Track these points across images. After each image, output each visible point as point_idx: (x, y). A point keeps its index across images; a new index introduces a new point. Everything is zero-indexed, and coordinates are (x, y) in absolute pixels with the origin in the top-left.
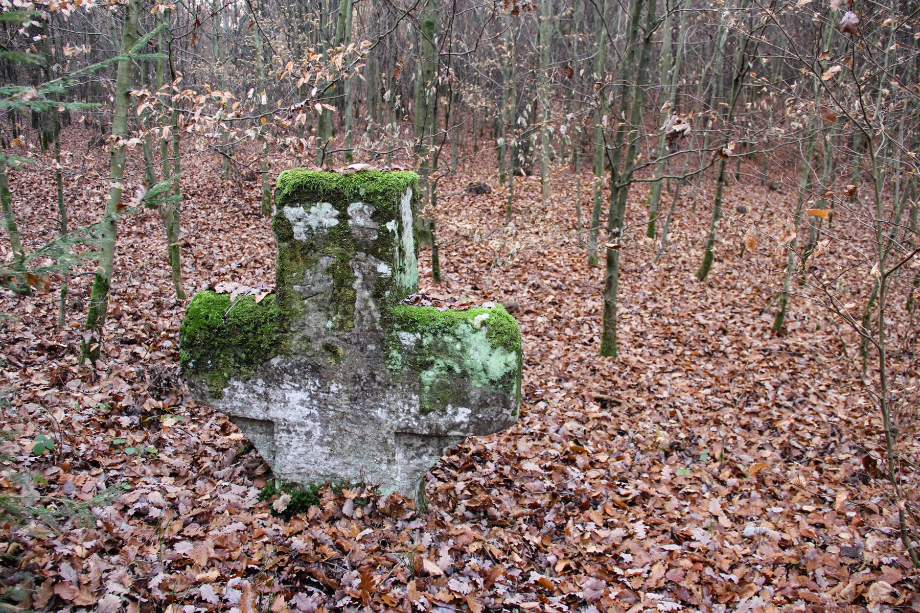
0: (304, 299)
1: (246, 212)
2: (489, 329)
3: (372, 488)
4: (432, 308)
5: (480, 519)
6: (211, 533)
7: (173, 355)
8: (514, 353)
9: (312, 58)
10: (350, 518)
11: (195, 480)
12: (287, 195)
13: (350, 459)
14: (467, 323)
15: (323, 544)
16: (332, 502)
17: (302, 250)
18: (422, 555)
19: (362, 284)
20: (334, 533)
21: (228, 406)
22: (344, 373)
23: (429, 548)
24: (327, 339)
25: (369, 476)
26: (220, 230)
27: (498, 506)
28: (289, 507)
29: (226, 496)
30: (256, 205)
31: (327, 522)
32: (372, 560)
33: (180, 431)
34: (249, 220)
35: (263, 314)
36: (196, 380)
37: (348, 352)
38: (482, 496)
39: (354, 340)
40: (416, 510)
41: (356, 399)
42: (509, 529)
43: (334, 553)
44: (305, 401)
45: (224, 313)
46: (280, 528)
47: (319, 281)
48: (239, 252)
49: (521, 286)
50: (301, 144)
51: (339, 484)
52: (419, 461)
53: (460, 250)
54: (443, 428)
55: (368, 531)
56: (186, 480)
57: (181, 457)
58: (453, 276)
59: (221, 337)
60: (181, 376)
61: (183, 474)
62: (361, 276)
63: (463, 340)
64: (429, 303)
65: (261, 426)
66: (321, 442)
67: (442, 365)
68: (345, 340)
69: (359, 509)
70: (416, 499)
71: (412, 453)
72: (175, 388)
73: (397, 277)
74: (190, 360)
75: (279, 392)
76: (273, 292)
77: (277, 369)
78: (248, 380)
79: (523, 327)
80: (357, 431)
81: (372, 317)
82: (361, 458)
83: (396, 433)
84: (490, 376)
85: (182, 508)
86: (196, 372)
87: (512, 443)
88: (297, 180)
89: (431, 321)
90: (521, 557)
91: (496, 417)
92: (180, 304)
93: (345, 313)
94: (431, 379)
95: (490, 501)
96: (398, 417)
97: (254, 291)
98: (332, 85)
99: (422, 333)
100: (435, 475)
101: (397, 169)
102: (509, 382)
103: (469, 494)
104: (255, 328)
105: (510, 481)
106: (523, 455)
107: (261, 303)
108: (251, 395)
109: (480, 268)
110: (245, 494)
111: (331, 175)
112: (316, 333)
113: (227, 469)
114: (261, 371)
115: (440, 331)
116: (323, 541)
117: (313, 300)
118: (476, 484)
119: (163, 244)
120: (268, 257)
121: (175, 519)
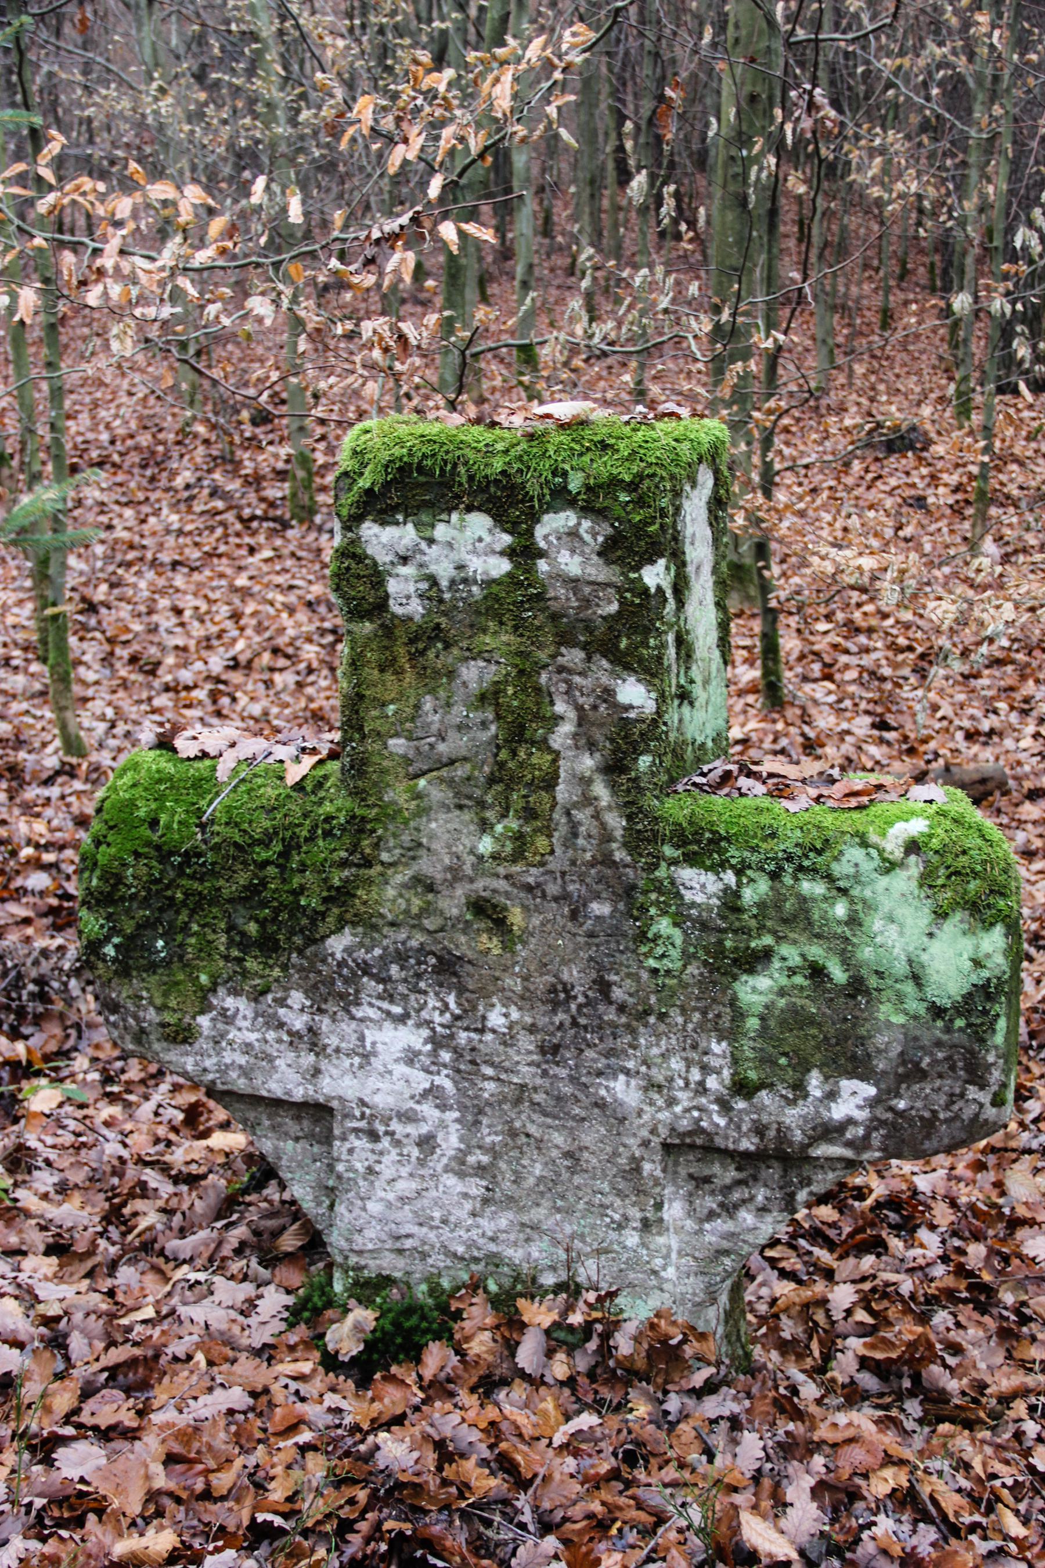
0: (417, 776)
1: (247, 512)
2: (927, 862)
3: (600, 1299)
4: (766, 802)
5: (900, 1396)
6: (157, 1418)
7: (52, 911)
8: (999, 930)
9: (427, 82)
10: (536, 1382)
11: (113, 1266)
12: (369, 492)
13: (537, 1214)
14: (864, 844)
15: (463, 1456)
16: (487, 1335)
17: (412, 641)
18: (738, 1499)
19: (575, 736)
20: (492, 1423)
21: (208, 1063)
22: (526, 979)
23: (757, 1477)
24: (480, 884)
25: (591, 1264)
26: (175, 565)
27: (952, 1361)
28: (370, 1346)
29: (199, 1313)
30: (273, 492)
31: (473, 1390)
32: (596, 1507)
33: (72, 1125)
34: (254, 533)
35: (305, 816)
36: (120, 993)
37: (536, 921)
38: (906, 1330)
39: (553, 889)
40: (718, 1364)
41: (556, 1049)
42: (987, 1434)
43: (493, 1482)
44: (417, 1053)
45: (200, 813)
46: (344, 1405)
47: (460, 728)
48: (229, 624)
49: (1014, 718)
50: (402, 339)
51: (507, 1282)
52: (729, 1226)
53: (840, 616)
54: (798, 1136)
55: (587, 1420)
56: (89, 1264)
57: (77, 1198)
58: (821, 691)
59: (192, 877)
60: (77, 972)
61: (81, 1248)
62: (572, 714)
63: (855, 892)
64: (760, 789)
65: (298, 1118)
66: (460, 1167)
67: (796, 960)
68: (529, 888)
69: (561, 1356)
70: (720, 1330)
71: (711, 1203)
72: (59, 1006)
73: (672, 716)
74: (107, 939)
75: (348, 1027)
76: (333, 755)
77: (341, 964)
78: (264, 992)
79: (1021, 837)
80: (558, 1138)
81: (603, 825)
82: (569, 1211)
83: (666, 1147)
84: (930, 992)
85: (77, 1344)
86: (124, 970)
87: (991, 1176)
88: (397, 451)
89: (764, 839)
90: (1026, 1522)
91: (947, 1107)
92: (68, 771)
93: (529, 814)
94: (763, 999)
95: (930, 1346)
96: (671, 1102)
97: (282, 752)
98: (481, 156)
99: (739, 873)
100: (773, 1262)
101: (672, 414)
102: (985, 1012)
103: (869, 1320)
104: (285, 854)
105: (989, 1290)
106: (1022, 1212)
107: (299, 787)
108: (271, 1035)
109: (895, 666)
110: (249, 1307)
111: (489, 436)
112: (450, 869)
113: (203, 1234)
114: (301, 969)
115: (789, 868)
116: (463, 1445)
117: (442, 780)
118: (887, 1292)
119: (20, 603)
120: (309, 640)
121: (59, 1377)
